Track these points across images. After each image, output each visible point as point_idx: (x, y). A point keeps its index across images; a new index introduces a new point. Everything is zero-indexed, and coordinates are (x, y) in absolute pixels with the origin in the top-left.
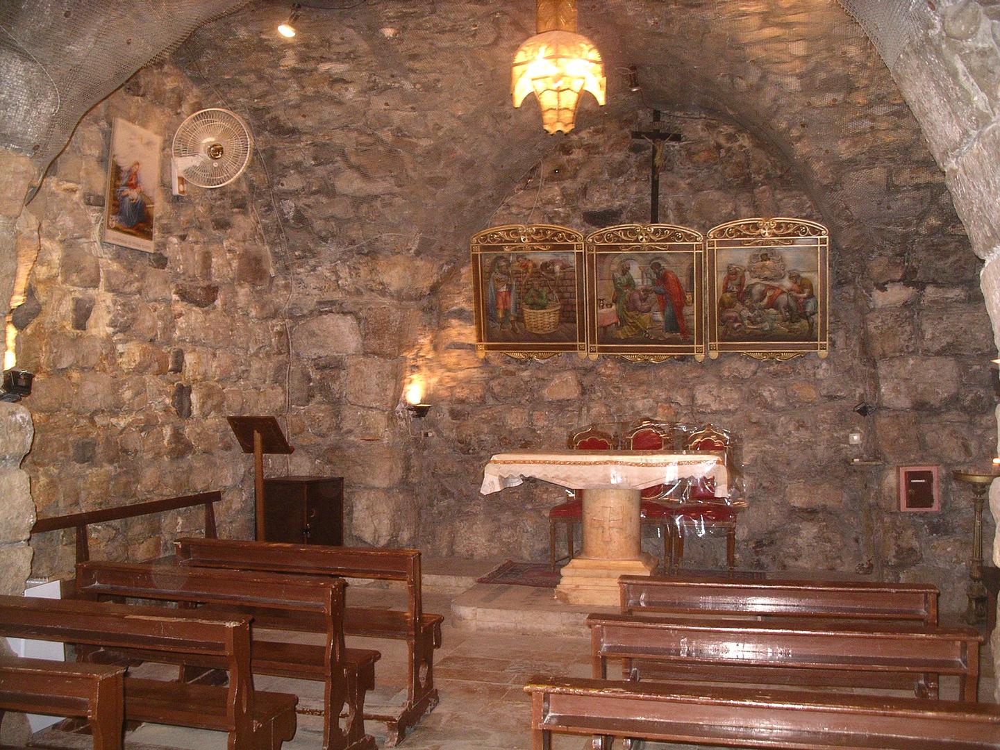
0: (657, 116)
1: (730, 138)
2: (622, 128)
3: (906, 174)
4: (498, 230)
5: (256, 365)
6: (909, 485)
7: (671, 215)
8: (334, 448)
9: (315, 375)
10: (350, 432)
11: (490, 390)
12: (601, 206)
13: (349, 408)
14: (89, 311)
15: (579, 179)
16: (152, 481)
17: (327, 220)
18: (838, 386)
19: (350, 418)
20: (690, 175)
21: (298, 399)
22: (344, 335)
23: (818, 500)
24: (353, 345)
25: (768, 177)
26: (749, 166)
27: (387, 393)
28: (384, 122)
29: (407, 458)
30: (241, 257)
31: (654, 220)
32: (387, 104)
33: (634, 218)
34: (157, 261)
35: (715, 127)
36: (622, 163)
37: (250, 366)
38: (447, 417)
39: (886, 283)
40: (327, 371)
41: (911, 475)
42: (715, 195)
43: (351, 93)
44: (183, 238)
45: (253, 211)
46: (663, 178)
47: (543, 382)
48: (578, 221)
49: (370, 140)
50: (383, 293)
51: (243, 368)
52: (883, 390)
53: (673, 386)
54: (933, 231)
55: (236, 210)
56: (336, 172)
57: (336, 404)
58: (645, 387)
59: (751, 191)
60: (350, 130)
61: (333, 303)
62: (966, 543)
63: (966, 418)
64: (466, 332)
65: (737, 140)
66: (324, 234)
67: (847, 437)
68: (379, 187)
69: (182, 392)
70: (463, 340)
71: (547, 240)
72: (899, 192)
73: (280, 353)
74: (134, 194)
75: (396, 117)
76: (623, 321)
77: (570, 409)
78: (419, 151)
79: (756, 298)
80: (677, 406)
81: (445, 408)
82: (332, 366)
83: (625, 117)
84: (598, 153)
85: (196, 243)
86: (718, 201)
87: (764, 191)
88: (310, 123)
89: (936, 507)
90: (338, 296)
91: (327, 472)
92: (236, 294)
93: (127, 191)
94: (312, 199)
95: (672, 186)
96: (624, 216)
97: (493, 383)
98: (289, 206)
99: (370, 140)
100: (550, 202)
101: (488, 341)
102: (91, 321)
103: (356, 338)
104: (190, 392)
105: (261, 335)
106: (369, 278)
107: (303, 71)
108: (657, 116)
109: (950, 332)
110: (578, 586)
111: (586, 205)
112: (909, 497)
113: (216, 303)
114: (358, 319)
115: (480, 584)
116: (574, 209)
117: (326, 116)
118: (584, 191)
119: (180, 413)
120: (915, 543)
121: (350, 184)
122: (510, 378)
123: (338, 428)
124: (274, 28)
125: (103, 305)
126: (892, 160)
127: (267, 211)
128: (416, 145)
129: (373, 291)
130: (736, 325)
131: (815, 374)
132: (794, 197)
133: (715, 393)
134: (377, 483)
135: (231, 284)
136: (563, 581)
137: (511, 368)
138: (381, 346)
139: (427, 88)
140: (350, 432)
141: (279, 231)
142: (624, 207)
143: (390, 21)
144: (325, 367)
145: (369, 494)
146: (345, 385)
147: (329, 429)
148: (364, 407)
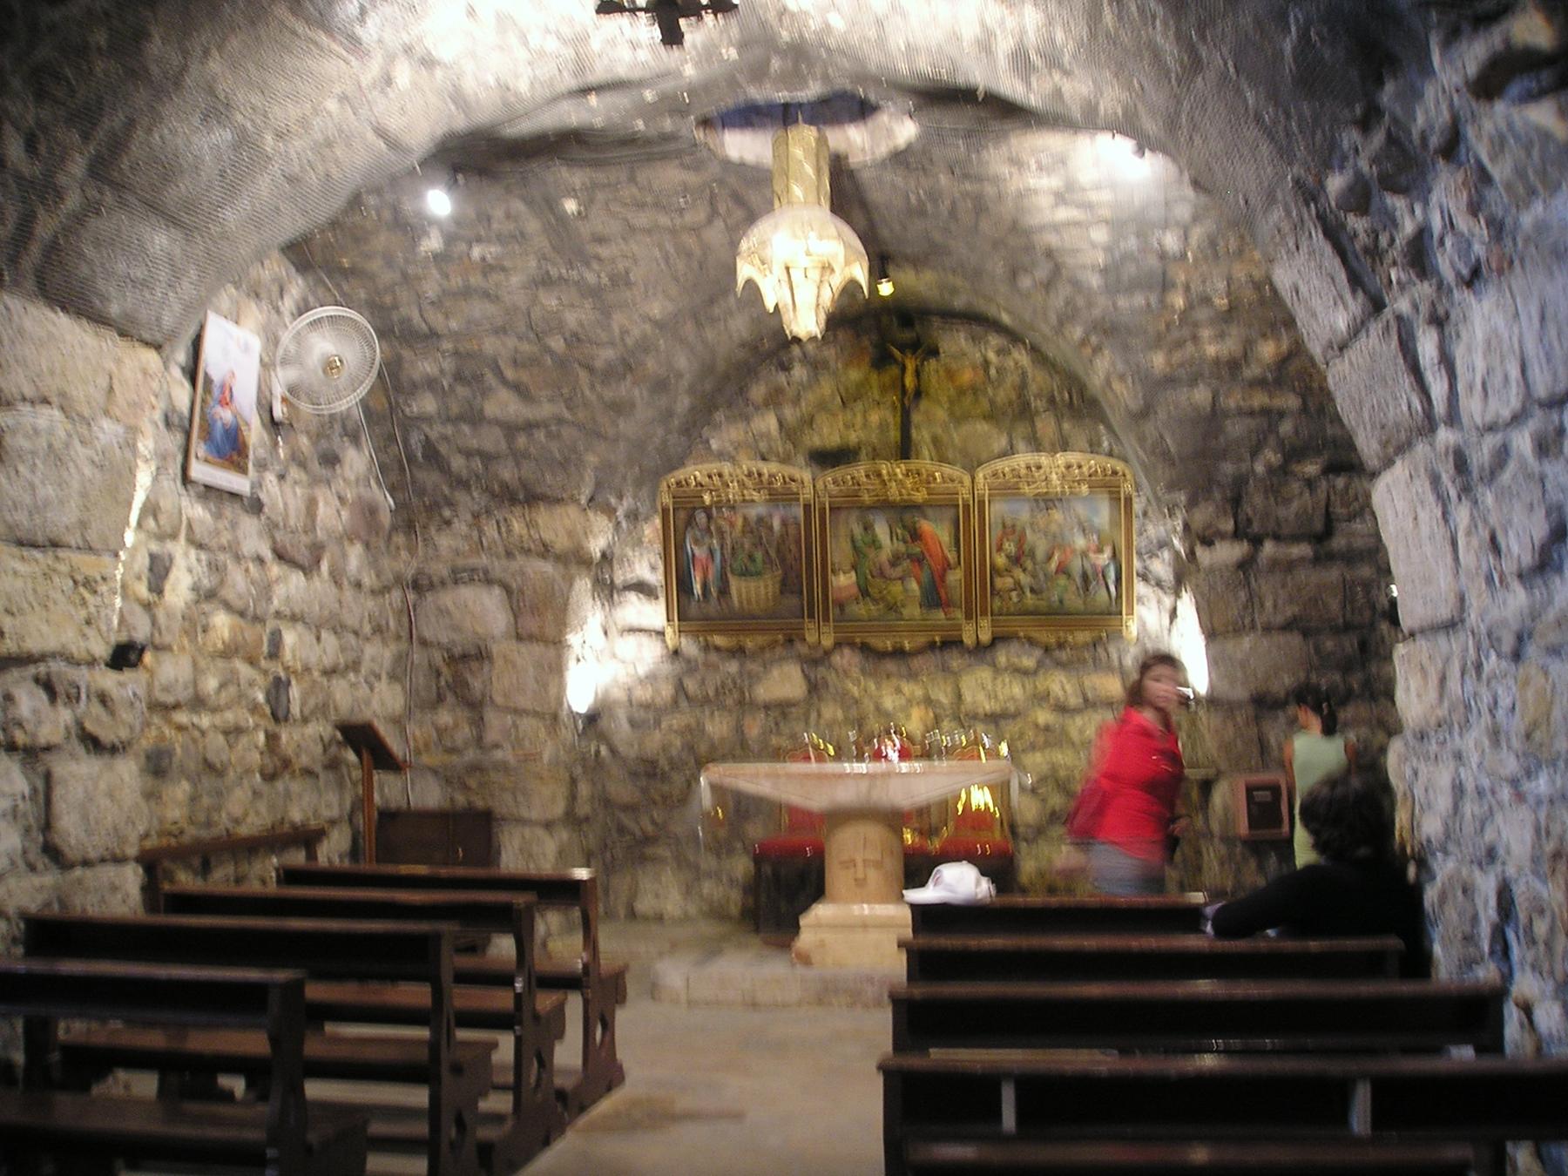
4: (695, 472)
8: (476, 768)
10: (497, 746)
14: (167, 571)
19: (496, 723)
22: (485, 611)
28: (555, 324)
29: (573, 782)
33: (875, 455)
34: (252, 507)
38: (626, 726)
42: (982, 427)
44: (281, 477)
47: (754, 678)
48: (801, 459)
56: (486, 392)
57: (475, 707)
64: (654, 613)
68: (546, 410)
69: (278, 687)
70: (646, 622)
74: (225, 415)
75: (571, 319)
76: (864, 592)
81: (622, 715)
88: (454, 324)
90: (483, 560)
92: (344, 556)
99: (535, 349)
104: (289, 683)
117: (477, 314)
118: (809, 421)
119: (276, 717)
121: (503, 404)
123: (479, 740)
124: (419, 196)
137: (1356, 681)
139: (615, 280)
140: (497, 746)
143: (572, 192)
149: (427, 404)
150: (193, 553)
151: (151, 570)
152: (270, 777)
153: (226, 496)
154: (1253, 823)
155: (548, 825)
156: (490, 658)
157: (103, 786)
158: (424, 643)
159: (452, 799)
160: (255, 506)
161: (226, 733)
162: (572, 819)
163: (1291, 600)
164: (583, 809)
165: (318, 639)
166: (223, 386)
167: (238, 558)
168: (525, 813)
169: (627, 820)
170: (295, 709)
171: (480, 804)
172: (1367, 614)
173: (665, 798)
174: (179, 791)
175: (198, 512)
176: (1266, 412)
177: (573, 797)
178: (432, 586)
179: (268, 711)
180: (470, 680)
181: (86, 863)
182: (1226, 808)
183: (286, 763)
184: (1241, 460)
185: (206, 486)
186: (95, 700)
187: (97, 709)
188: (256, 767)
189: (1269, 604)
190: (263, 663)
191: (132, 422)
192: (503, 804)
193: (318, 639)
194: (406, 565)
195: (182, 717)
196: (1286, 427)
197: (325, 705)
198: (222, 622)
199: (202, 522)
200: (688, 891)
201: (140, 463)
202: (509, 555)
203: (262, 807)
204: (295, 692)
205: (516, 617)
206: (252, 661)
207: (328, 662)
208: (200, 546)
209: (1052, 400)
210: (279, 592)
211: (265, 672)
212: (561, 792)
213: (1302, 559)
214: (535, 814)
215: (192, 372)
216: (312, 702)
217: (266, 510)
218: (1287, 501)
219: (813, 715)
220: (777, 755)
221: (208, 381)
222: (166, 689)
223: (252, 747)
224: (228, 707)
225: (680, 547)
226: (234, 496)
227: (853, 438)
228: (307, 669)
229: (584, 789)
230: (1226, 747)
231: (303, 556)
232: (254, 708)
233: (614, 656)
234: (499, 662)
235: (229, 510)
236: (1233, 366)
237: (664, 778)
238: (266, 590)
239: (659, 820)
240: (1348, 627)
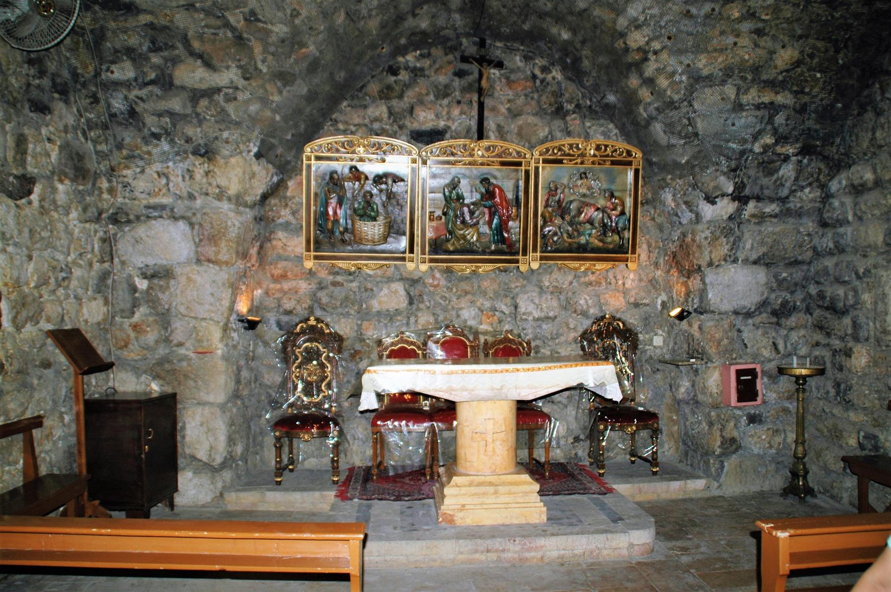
0: (482, 44)
1: (544, 69)
2: (446, 54)
3: (753, 92)
5: (77, 272)
6: (739, 381)
7: (491, 134)
8: (161, 362)
9: (142, 284)
10: (180, 345)
11: (318, 301)
12: (427, 125)
13: (180, 319)
15: (406, 99)
17: (160, 115)
18: (643, 294)
20: (509, 101)
25: (578, 106)
26: (562, 95)
27: (223, 303)
29: (239, 370)
35: (532, 58)
36: (447, 86)
37: (71, 273)
39: (717, 197)
40: (156, 281)
41: (739, 373)
42: (531, 119)
45: (76, 101)
46: (488, 102)
49: (219, 23)
50: (219, 197)
51: (63, 275)
52: (710, 296)
53: (497, 295)
54: (766, 148)
56: (175, 61)
58: (469, 297)
59: (563, 118)
60: (197, 10)
61: (163, 207)
62: (777, 431)
63: (774, 320)
65: (550, 72)
72: (743, 110)
73: (102, 261)
77: (399, 318)
78: (273, 39)
79: (573, 213)
80: (502, 315)
82: (160, 275)
83: (449, 44)
84: (424, 76)
86: (536, 125)
87: (574, 119)
91: (169, 390)
92: (54, 190)
94: (143, 93)
95: (493, 109)
96: (448, 135)
97: (320, 294)
100: (376, 120)
103: (188, 246)
105: (83, 240)
108: (482, 44)
110: (463, 506)
111: (412, 123)
112: (739, 391)
113: (32, 197)
114: (192, 225)
120: (735, 434)
122: (337, 289)
123: (167, 340)
126: (744, 79)
127: (92, 103)
128: (271, 31)
129: (207, 194)
130: (555, 239)
131: (624, 284)
132: (602, 125)
133: (537, 301)
134: (211, 398)
136: (447, 501)
140: (180, 345)
141: (105, 127)
144: (153, 276)
145: (203, 409)
146: (177, 296)
147: (157, 342)
148: (196, 318)
163: (762, 243)
178: (129, 222)
219: (412, 319)
227: (442, 124)
234: (183, 280)
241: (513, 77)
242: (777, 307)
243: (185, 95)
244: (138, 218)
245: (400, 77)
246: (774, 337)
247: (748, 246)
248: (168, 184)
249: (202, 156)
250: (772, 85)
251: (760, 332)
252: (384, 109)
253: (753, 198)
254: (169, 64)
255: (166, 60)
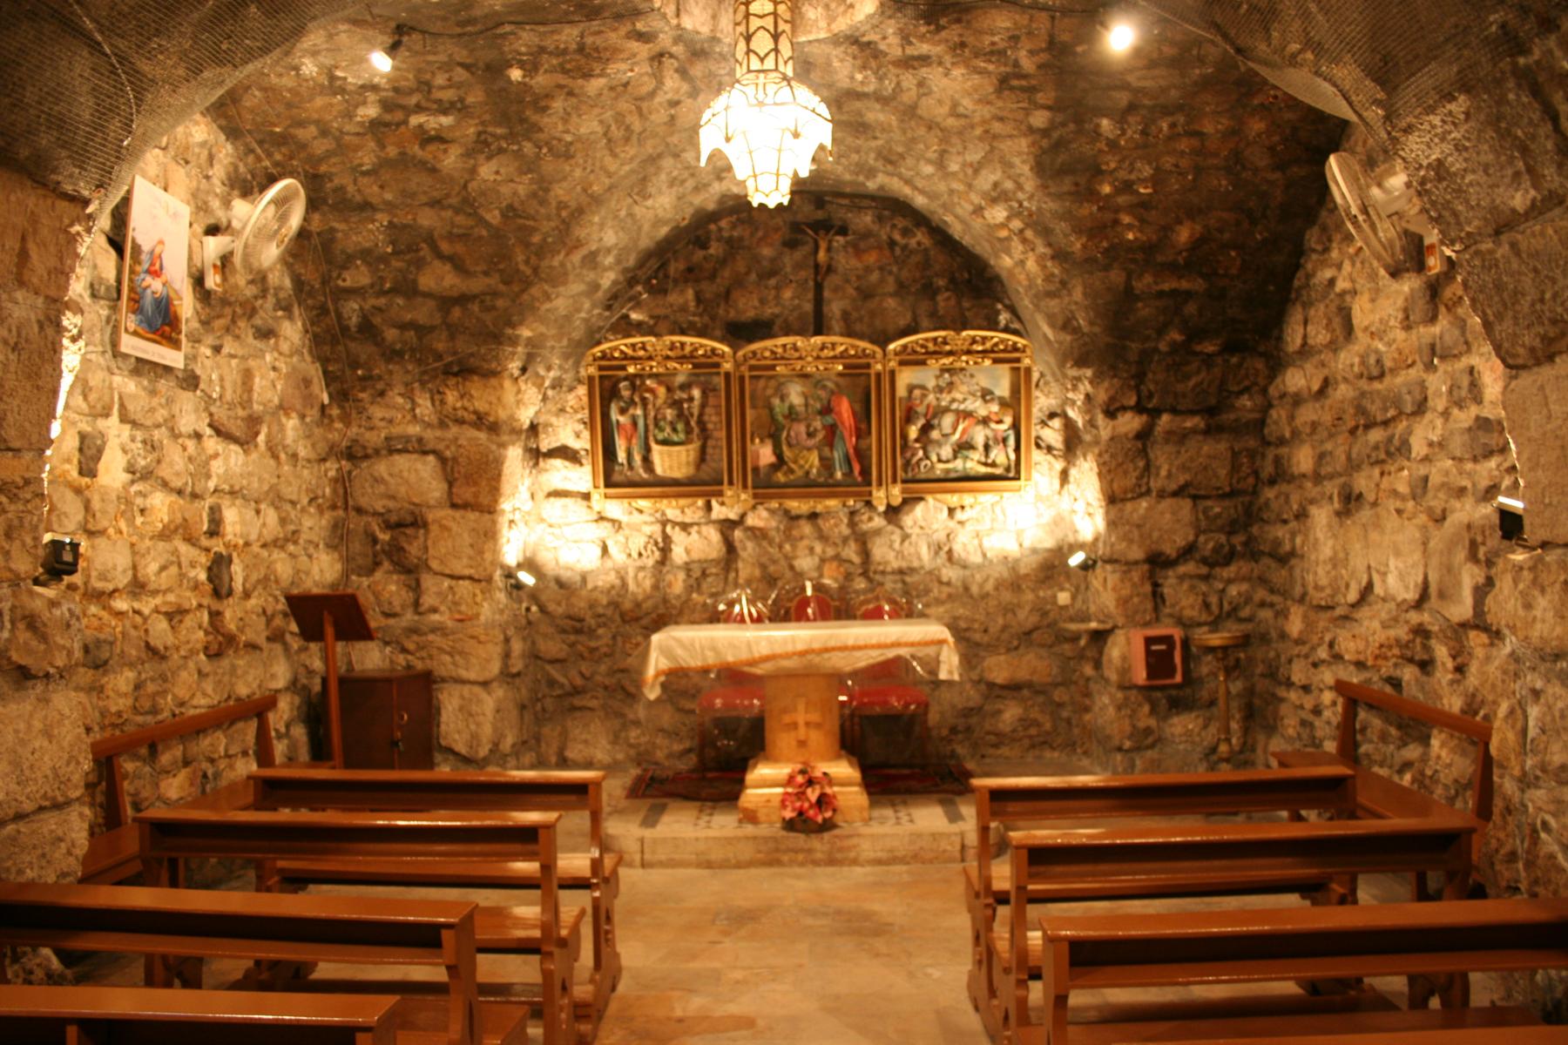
6: (1148, 653)
7: (837, 327)
9: (384, 537)
14: (100, 451)
15: (718, 280)
16: (195, 690)
21: (360, 567)
22: (418, 478)
23: (1022, 674)
24: (437, 494)
29: (507, 640)
30: (288, 376)
31: (818, 331)
32: (497, 173)
43: (451, 160)
44: (217, 349)
55: (280, 313)
56: (420, 264)
60: (444, 208)
63: (1204, 570)
65: (914, 235)
66: (398, 346)
67: (1055, 597)
68: (477, 285)
69: (218, 566)
71: (684, 357)
74: (156, 285)
85: (233, 356)
88: (388, 196)
89: (1178, 678)
92: (282, 428)
93: (149, 280)
98: (352, 310)
99: (471, 222)
101: (870, 484)
102: (101, 466)
104: (230, 561)
106: (459, 405)
107: (387, 125)
109: (1189, 469)
112: (1149, 666)
115: (799, 839)
116: (713, 318)
119: (217, 594)
121: (438, 278)
123: (417, 604)
125: (117, 441)
126: (1133, 261)
135: (273, 414)
137: (1237, 540)
138: (476, 495)
140: (434, 610)
142: (777, 316)
149: (357, 276)
150: (126, 430)
151: (81, 450)
152: (214, 655)
153: (160, 371)
154: (1152, 672)
155: (485, 684)
156: (425, 525)
157: (37, 724)
158: (360, 510)
159: (392, 661)
160: (190, 381)
161: (169, 616)
162: (508, 676)
164: (517, 665)
165: (258, 512)
166: (152, 252)
167: (175, 435)
168: (464, 674)
169: (553, 671)
170: (238, 585)
171: (419, 665)
172: (1251, 480)
173: (593, 650)
174: (122, 680)
175: (128, 385)
176: (1174, 293)
177: (507, 655)
178: (366, 457)
179: (208, 587)
180: (406, 546)
181: (19, 817)
182: (1124, 658)
183: (231, 640)
184: (1148, 338)
185: (138, 360)
186: (21, 626)
187: (24, 635)
188: (199, 646)
189: (1163, 473)
190: (205, 542)
191: (53, 293)
192: (443, 665)
193: (258, 512)
194: (339, 433)
195: (121, 604)
196: (1191, 309)
197: (266, 578)
198: (161, 505)
199: (135, 397)
200: (615, 741)
201: (66, 342)
202: (442, 425)
203: (208, 686)
204: (237, 569)
205: (451, 485)
206: (190, 540)
207: (268, 536)
208: (135, 424)
209: (952, 280)
210: (217, 467)
211: (208, 550)
212: (496, 651)
213: (1194, 431)
214: (472, 676)
215: (117, 241)
216: (254, 577)
217: (202, 386)
218: (1188, 377)
220: (715, 618)
221: (137, 249)
222: (103, 577)
223: (195, 632)
224: (169, 590)
225: (606, 416)
226: (168, 370)
227: (769, 311)
228: (247, 544)
229: (517, 646)
230: (1123, 602)
231: (237, 429)
232: (196, 587)
233: (542, 520)
234: (434, 528)
235: (163, 385)
236: (1149, 249)
237: (591, 633)
238: (202, 469)
239: (587, 674)
240: (1232, 494)
241: (862, 245)
242: (1207, 553)
243: (431, 303)
244: (377, 452)
245: (712, 251)
246: (1204, 594)
247: (1163, 473)
248: (413, 410)
249: (456, 375)
250: (1173, 269)
251: (1185, 586)
252: (690, 294)
253: (1166, 411)
254: (412, 268)
255: (409, 263)
